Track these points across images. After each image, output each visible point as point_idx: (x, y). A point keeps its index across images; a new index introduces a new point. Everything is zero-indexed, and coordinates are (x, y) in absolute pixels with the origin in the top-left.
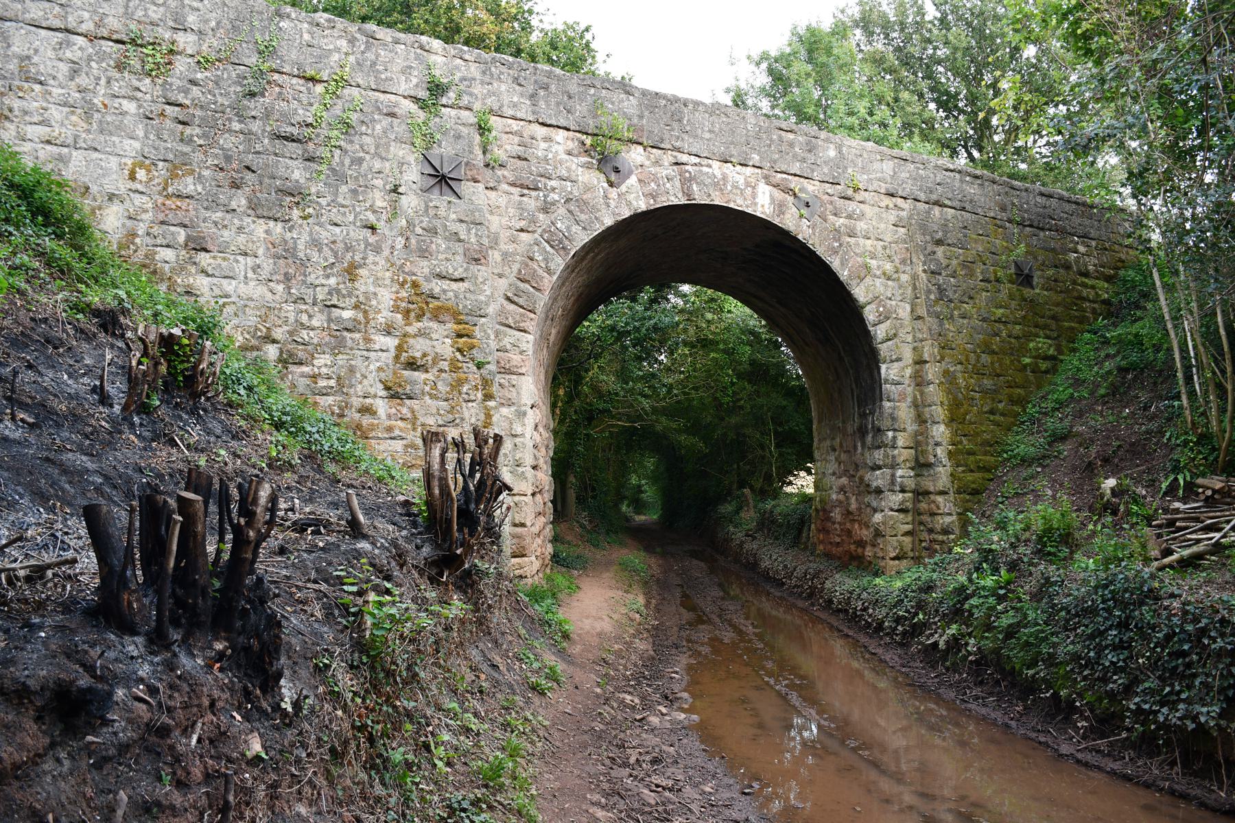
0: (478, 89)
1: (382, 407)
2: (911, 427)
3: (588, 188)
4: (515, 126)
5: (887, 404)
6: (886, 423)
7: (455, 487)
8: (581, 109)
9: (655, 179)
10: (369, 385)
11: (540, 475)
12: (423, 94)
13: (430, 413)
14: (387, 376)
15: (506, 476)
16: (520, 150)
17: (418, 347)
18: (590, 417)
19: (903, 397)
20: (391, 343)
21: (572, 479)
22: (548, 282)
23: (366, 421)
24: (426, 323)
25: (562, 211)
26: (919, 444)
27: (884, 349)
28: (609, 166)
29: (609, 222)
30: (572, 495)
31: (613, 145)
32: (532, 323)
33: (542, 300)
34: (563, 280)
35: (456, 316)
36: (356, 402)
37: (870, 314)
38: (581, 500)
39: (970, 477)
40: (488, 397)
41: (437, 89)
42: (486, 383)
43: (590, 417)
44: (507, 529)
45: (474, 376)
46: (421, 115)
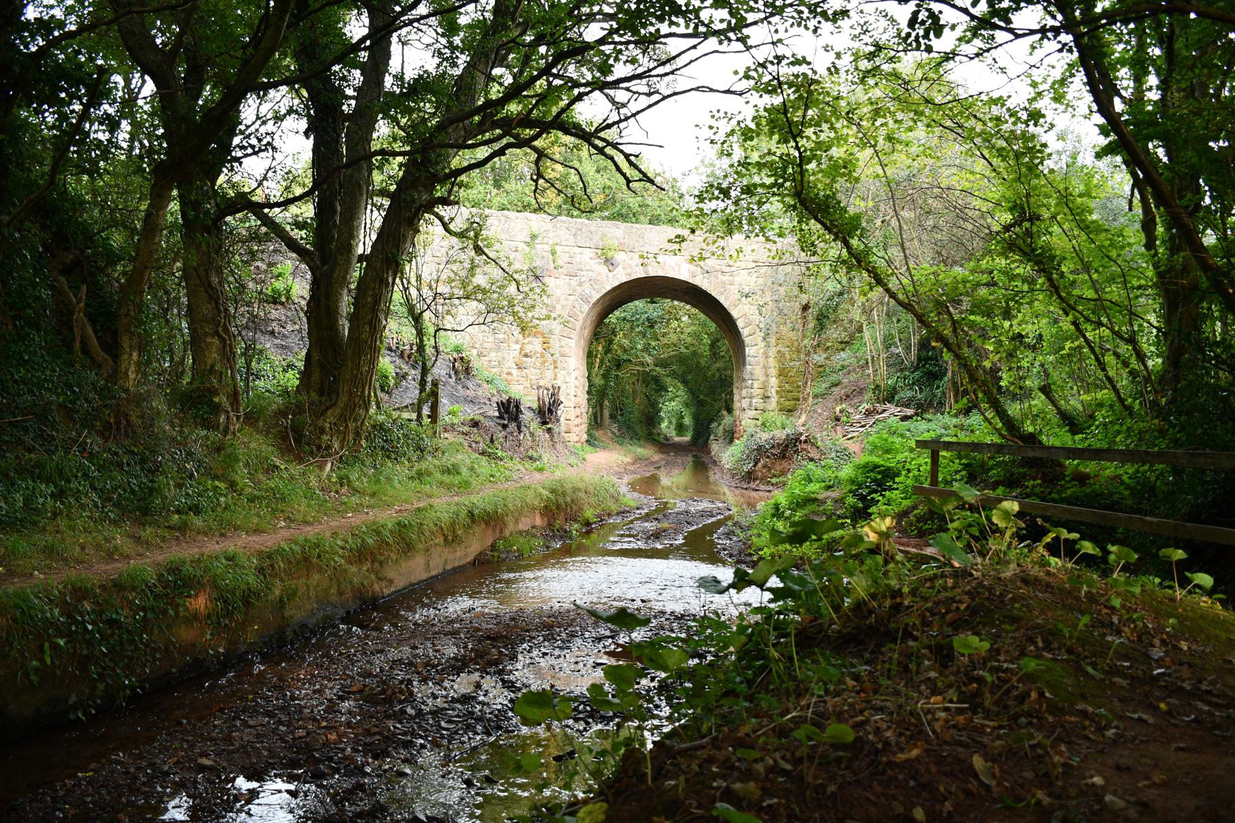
0: (551, 235)
1: (515, 372)
2: (762, 379)
3: (599, 274)
4: (567, 249)
5: (748, 367)
6: (746, 377)
7: (547, 400)
8: (596, 238)
9: (630, 266)
10: (510, 364)
11: (578, 399)
12: (528, 240)
13: (533, 374)
14: (517, 360)
15: (562, 398)
16: (569, 260)
17: (528, 349)
18: (618, 364)
19: (758, 363)
20: (518, 347)
21: (606, 403)
22: (581, 317)
23: (509, 377)
24: (530, 339)
25: (587, 285)
26: (764, 387)
27: (747, 341)
28: (609, 262)
29: (609, 288)
30: (606, 413)
31: (610, 254)
32: (574, 335)
33: (579, 324)
34: (588, 314)
35: (543, 334)
36: (506, 371)
37: (740, 324)
38: (612, 417)
39: (787, 403)
40: (556, 368)
41: (534, 237)
42: (555, 362)
43: (618, 364)
44: (562, 419)
45: (550, 359)
46: (528, 249)
